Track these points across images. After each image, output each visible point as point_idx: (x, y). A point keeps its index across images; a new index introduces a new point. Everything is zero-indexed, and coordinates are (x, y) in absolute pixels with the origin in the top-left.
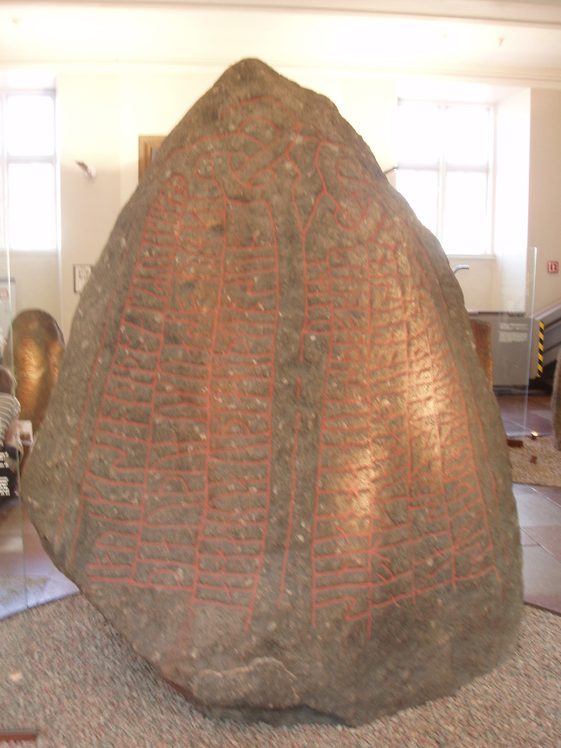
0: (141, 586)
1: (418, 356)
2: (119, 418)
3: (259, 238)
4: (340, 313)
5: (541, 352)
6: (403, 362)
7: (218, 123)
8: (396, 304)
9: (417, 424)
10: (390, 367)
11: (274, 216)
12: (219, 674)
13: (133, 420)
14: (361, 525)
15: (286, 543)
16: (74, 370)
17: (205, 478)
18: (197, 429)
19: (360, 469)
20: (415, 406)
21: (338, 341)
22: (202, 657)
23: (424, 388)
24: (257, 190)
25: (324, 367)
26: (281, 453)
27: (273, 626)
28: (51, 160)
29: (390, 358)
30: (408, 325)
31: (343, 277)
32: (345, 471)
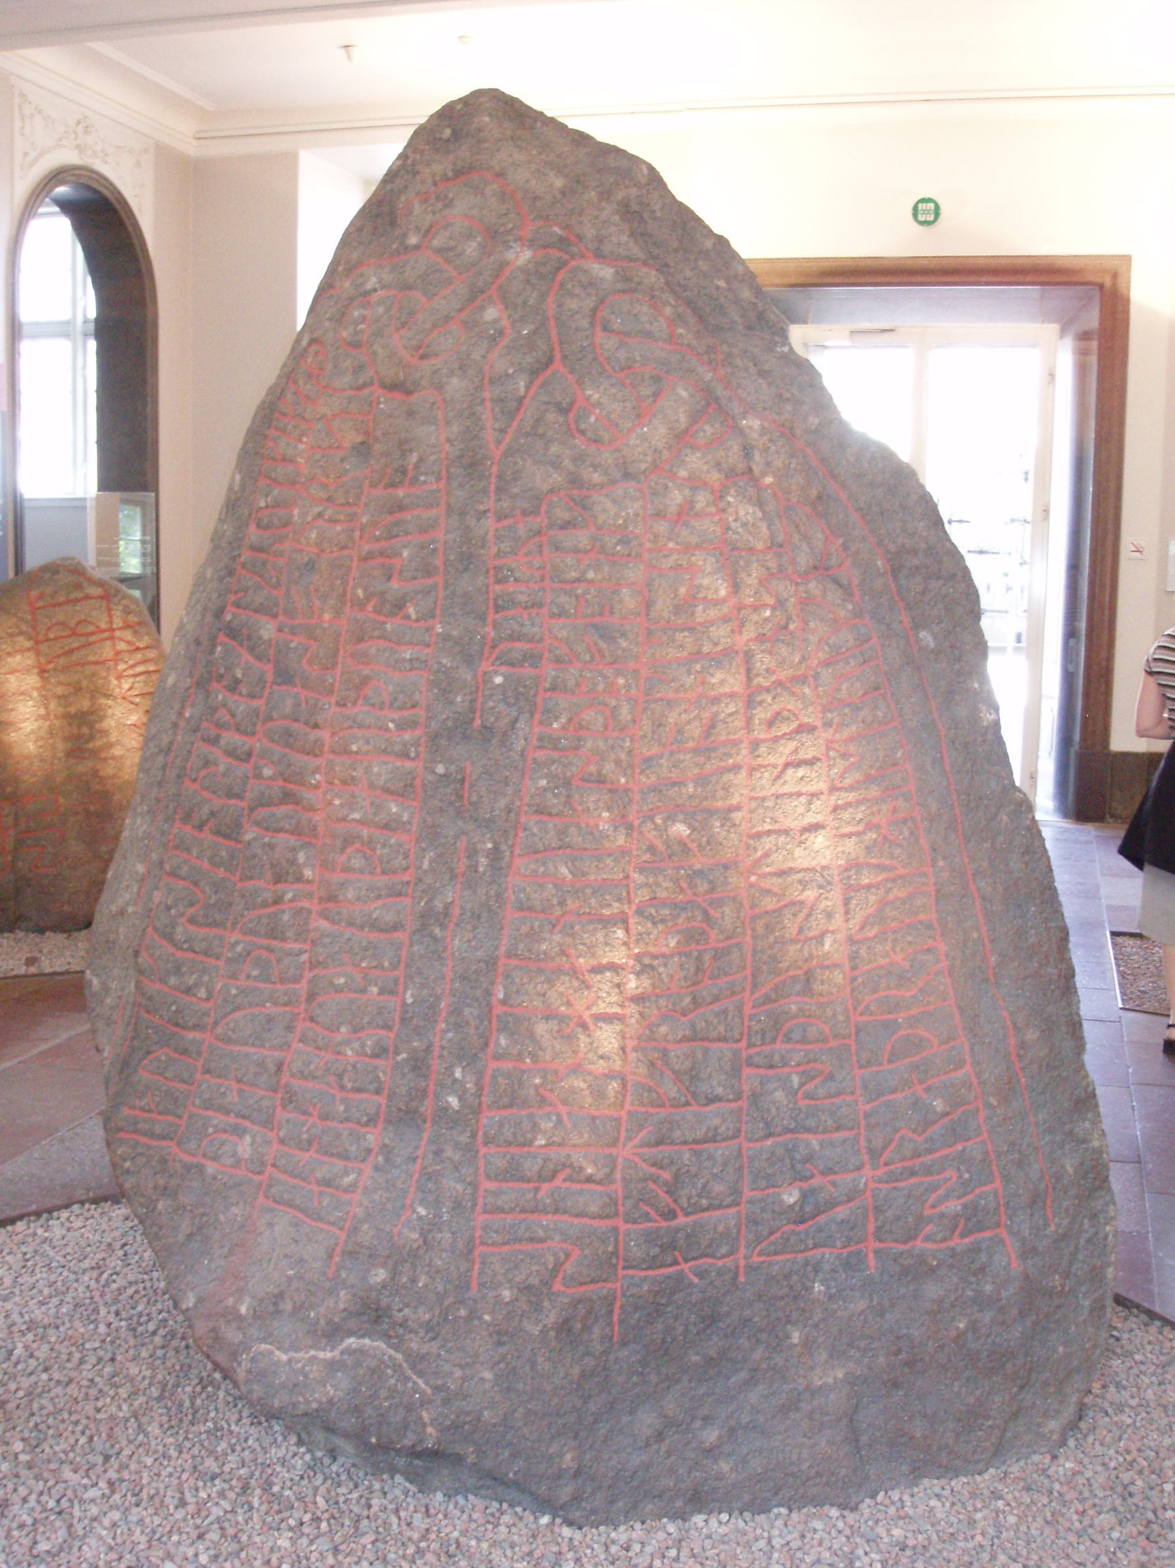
0: (188, 1159)
1: (777, 732)
2: (200, 827)
4: (561, 629)
6: (735, 743)
8: (713, 613)
9: (774, 883)
10: (696, 751)
12: (284, 1358)
14: (599, 1094)
15: (427, 1108)
18: (301, 857)
19: (598, 969)
20: (768, 843)
21: (554, 688)
22: (256, 1315)
23: (799, 804)
24: (427, 366)
25: (519, 745)
26: (426, 918)
27: (380, 1275)
29: (695, 730)
30: (748, 657)
31: (577, 551)
32: (560, 970)
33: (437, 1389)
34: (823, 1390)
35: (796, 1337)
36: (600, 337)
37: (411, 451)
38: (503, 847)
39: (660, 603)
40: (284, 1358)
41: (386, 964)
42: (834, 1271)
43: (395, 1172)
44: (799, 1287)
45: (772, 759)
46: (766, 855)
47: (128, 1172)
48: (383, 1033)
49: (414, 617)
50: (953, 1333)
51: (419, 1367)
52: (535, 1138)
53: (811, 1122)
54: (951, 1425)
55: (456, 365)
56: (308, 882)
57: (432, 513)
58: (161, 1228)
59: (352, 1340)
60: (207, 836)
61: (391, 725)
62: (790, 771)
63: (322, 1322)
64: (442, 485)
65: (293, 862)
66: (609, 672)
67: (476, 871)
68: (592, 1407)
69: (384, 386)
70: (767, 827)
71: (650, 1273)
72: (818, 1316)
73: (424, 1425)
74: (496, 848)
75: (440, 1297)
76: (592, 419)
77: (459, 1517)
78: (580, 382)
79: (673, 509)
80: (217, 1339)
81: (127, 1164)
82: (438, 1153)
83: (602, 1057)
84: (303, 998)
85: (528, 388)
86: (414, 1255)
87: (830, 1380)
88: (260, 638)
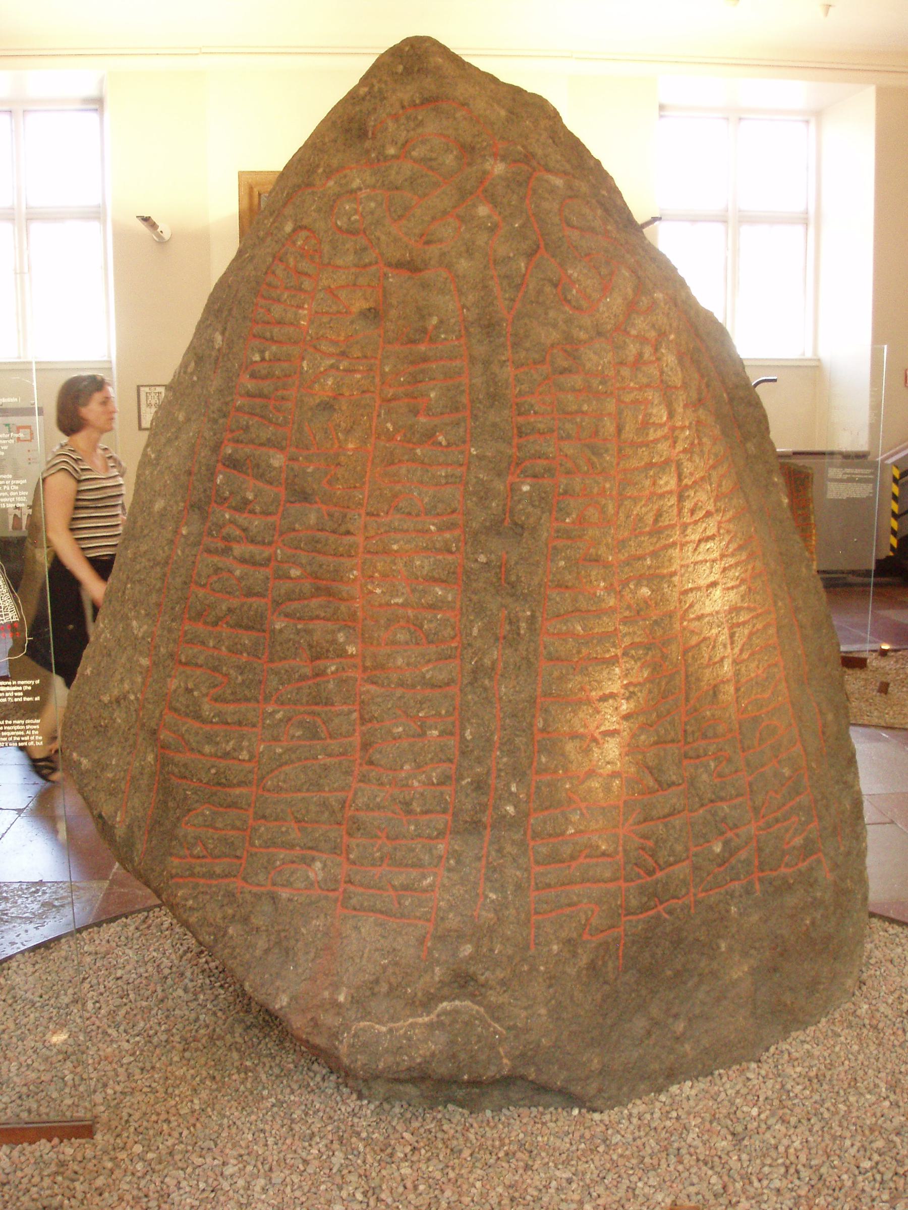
0: (255, 890)
3: (436, 327)
4: (569, 448)
5: (895, 516)
7: (368, 144)
10: (650, 534)
11: (460, 292)
12: (384, 1029)
13: (238, 625)
14: (607, 789)
16: (143, 548)
17: (355, 715)
18: (341, 637)
19: (604, 698)
20: (691, 598)
22: (354, 1000)
24: (434, 251)
27: (467, 950)
28: (97, 214)
29: (650, 519)
30: (679, 465)
31: (573, 390)
32: (580, 702)
33: (509, 1028)
34: (740, 979)
35: (723, 946)
36: (568, 232)
37: (430, 315)
38: (538, 614)
39: (627, 428)
40: (384, 1029)
41: (443, 712)
42: (741, 896)
43: (467, 870)
44: (723, 912)
45: (693, 537)
46: (691, 606)
47: (191, 909)
48: (445, 766)
49: (444, 443)
50: (804, 928)
51: (496, 1014)
52: (567, 829)
53: (723, 794)
54: (803, 992)
55: (463, 249)
56: (352, 656)
57: (458, 363)
58: (234, 948)
59: (445, 1004)
60: (225, 631)
61: (432, 528)
62: (702, 545)
63: (420, 994)
64: (463, 341)
65: (334, 641)
66: (600, 479)
67: (519, 634)
68: (609, 1022)
69: (389, 265)
70: (690, 586)
71: (641, 916)
72: (733, 930)
73: (501, 1058)
74: (533, 616)
75: (510, 958)
76: (574, 292)
77: (516, 1124)
78: (561, 265)
79: (631, 359)
80: (316, 1025)
81: (191, 902)
82: (500, 850)
83: (608, 763)
84: (358, 748)
85: (527, 268)
86: (491, 930)
87: (741, 974)
88: (269, 466)
